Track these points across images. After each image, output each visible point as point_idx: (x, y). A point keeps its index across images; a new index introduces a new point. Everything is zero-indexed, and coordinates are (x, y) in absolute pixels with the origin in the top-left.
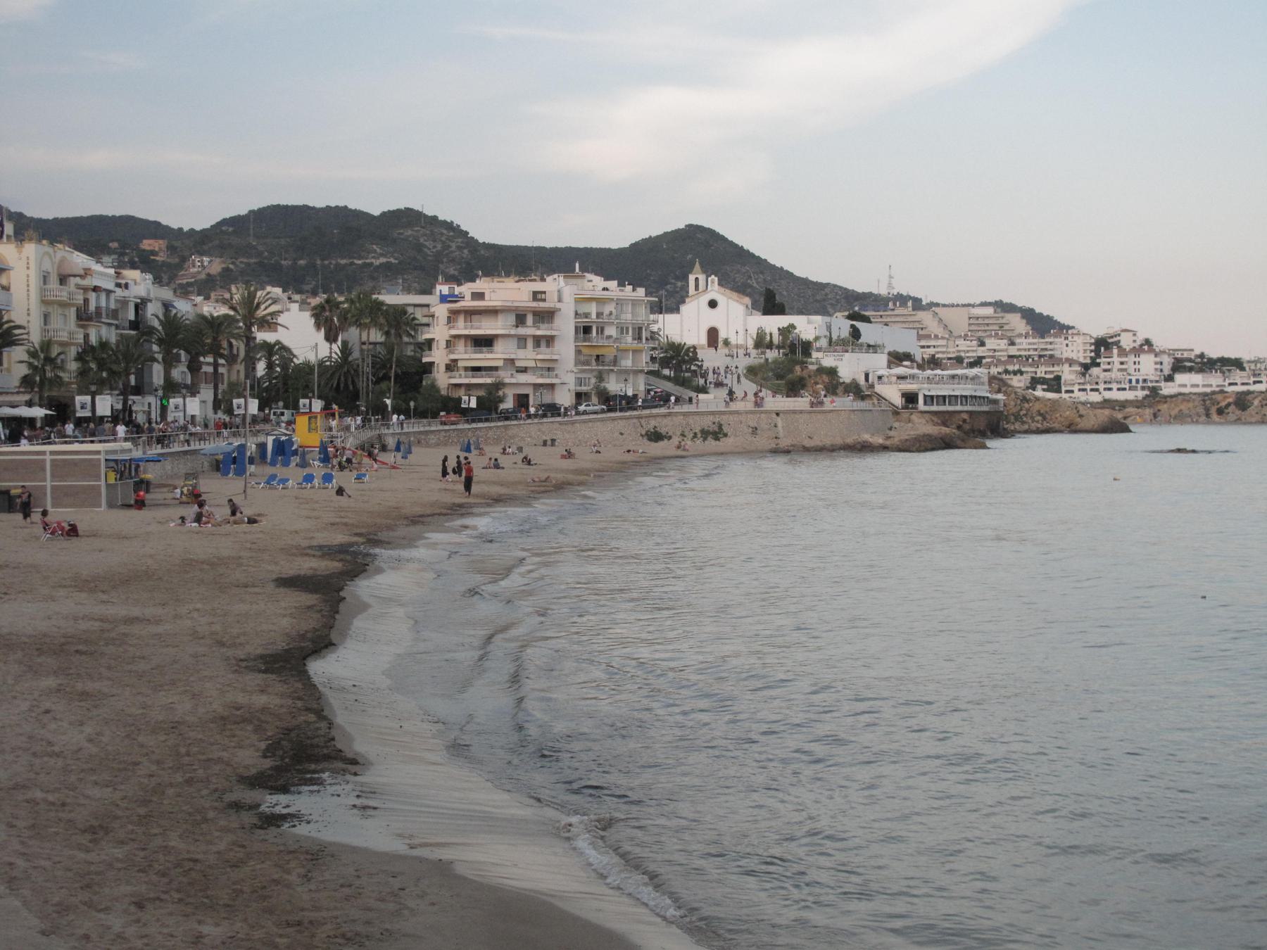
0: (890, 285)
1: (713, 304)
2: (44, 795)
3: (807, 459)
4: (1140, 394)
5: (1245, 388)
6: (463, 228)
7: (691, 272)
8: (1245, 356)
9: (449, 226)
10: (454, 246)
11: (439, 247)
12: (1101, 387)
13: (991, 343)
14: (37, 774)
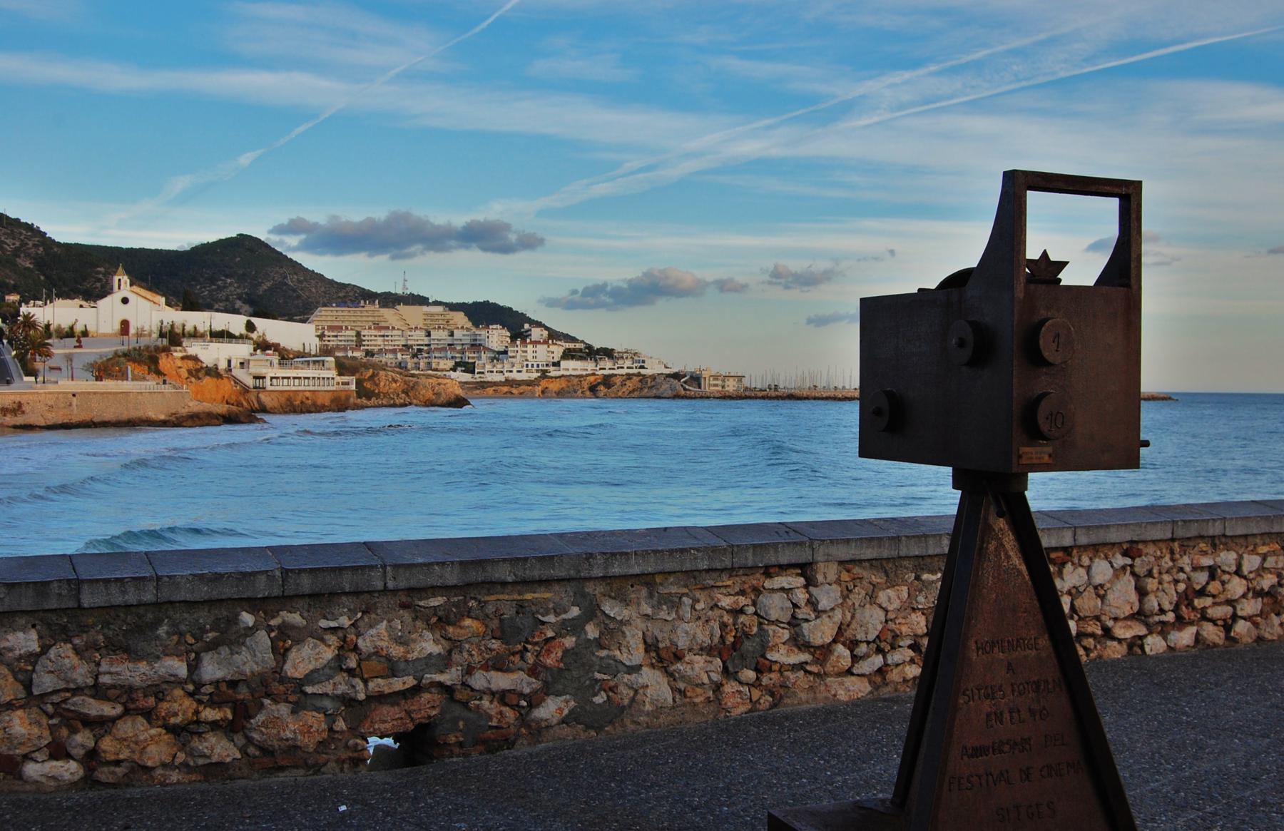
0: (405, 287)
1: (125, 301)
2: (611, 653)
3: (111, 431)
4: (536, 375)
5: (612, 372)
6: (42, 229)
7: (115, 273)
8: (618, 347)
9: (29, 227)
10: (30, 243)
11: (18, 244)
12: (515, 369)
13: (434, 334)
14: (1238, 572)
